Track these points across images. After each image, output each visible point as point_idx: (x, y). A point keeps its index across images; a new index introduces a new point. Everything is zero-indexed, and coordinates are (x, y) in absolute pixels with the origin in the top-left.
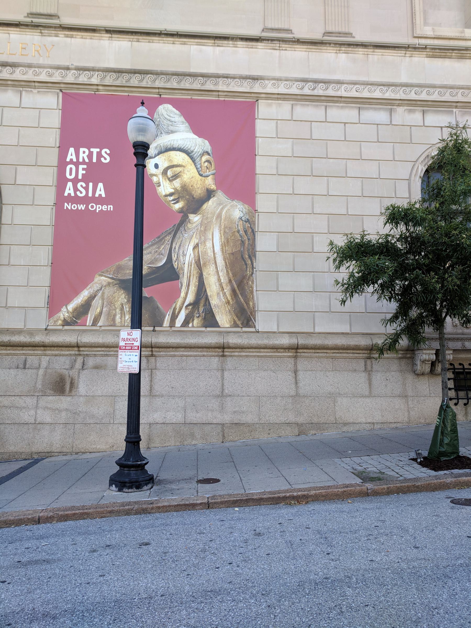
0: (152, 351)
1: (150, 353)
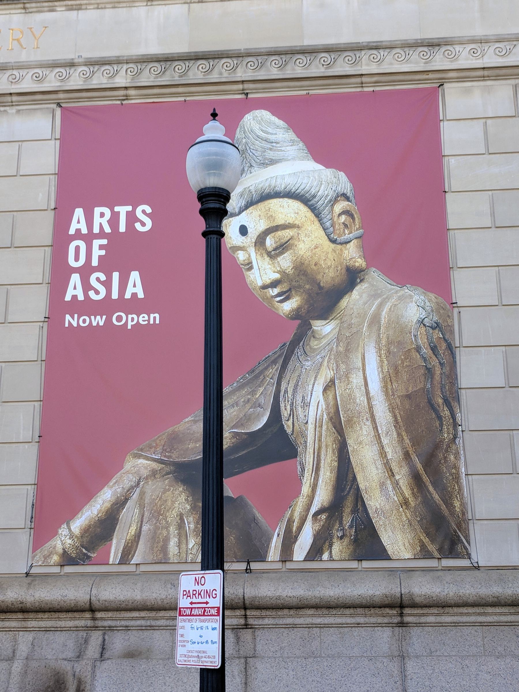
1: (242, 621)
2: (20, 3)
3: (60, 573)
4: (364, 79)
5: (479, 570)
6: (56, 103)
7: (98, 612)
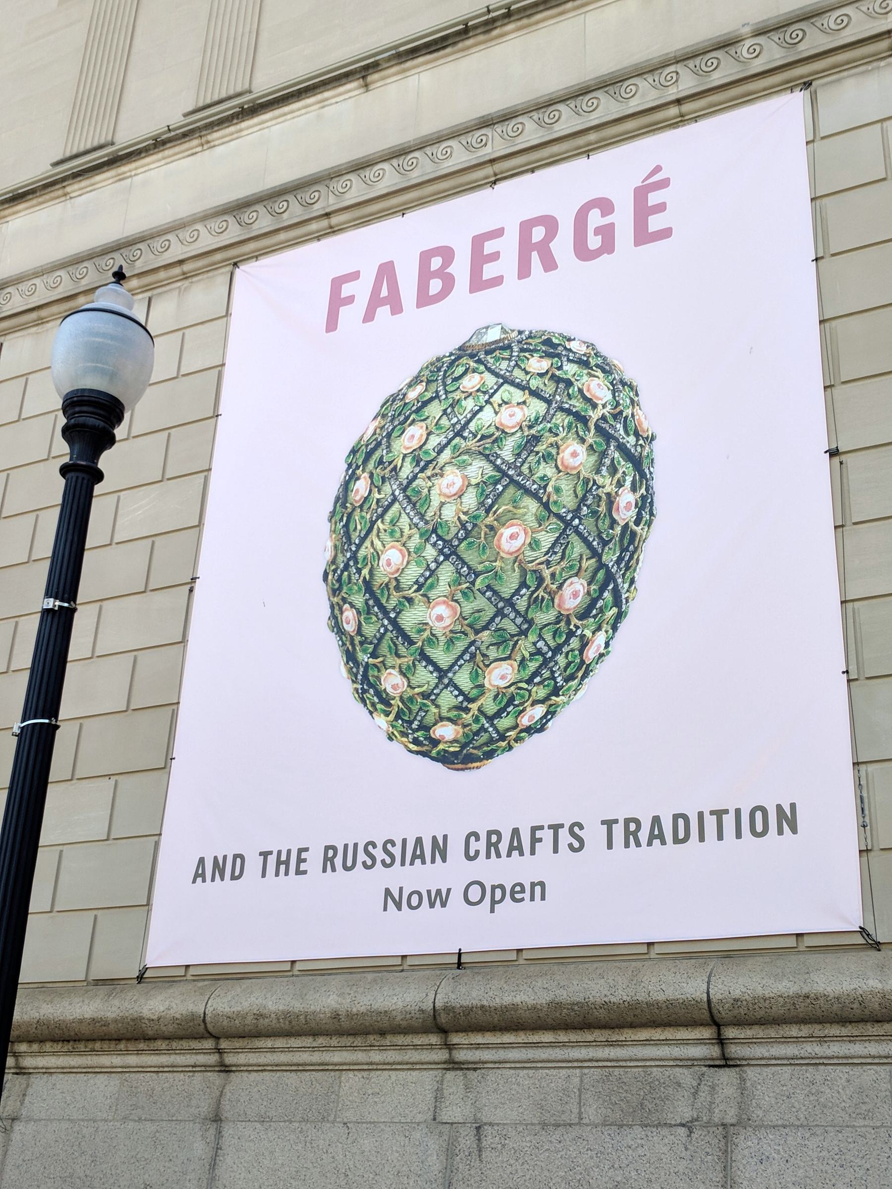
0: (721, 1042)
1: (715, 1051)
2: (195, 138)
3: (184, 976)
4: (187, 267)
5: (879, 950)
6: (230, 264)
7: (454, 1034)
